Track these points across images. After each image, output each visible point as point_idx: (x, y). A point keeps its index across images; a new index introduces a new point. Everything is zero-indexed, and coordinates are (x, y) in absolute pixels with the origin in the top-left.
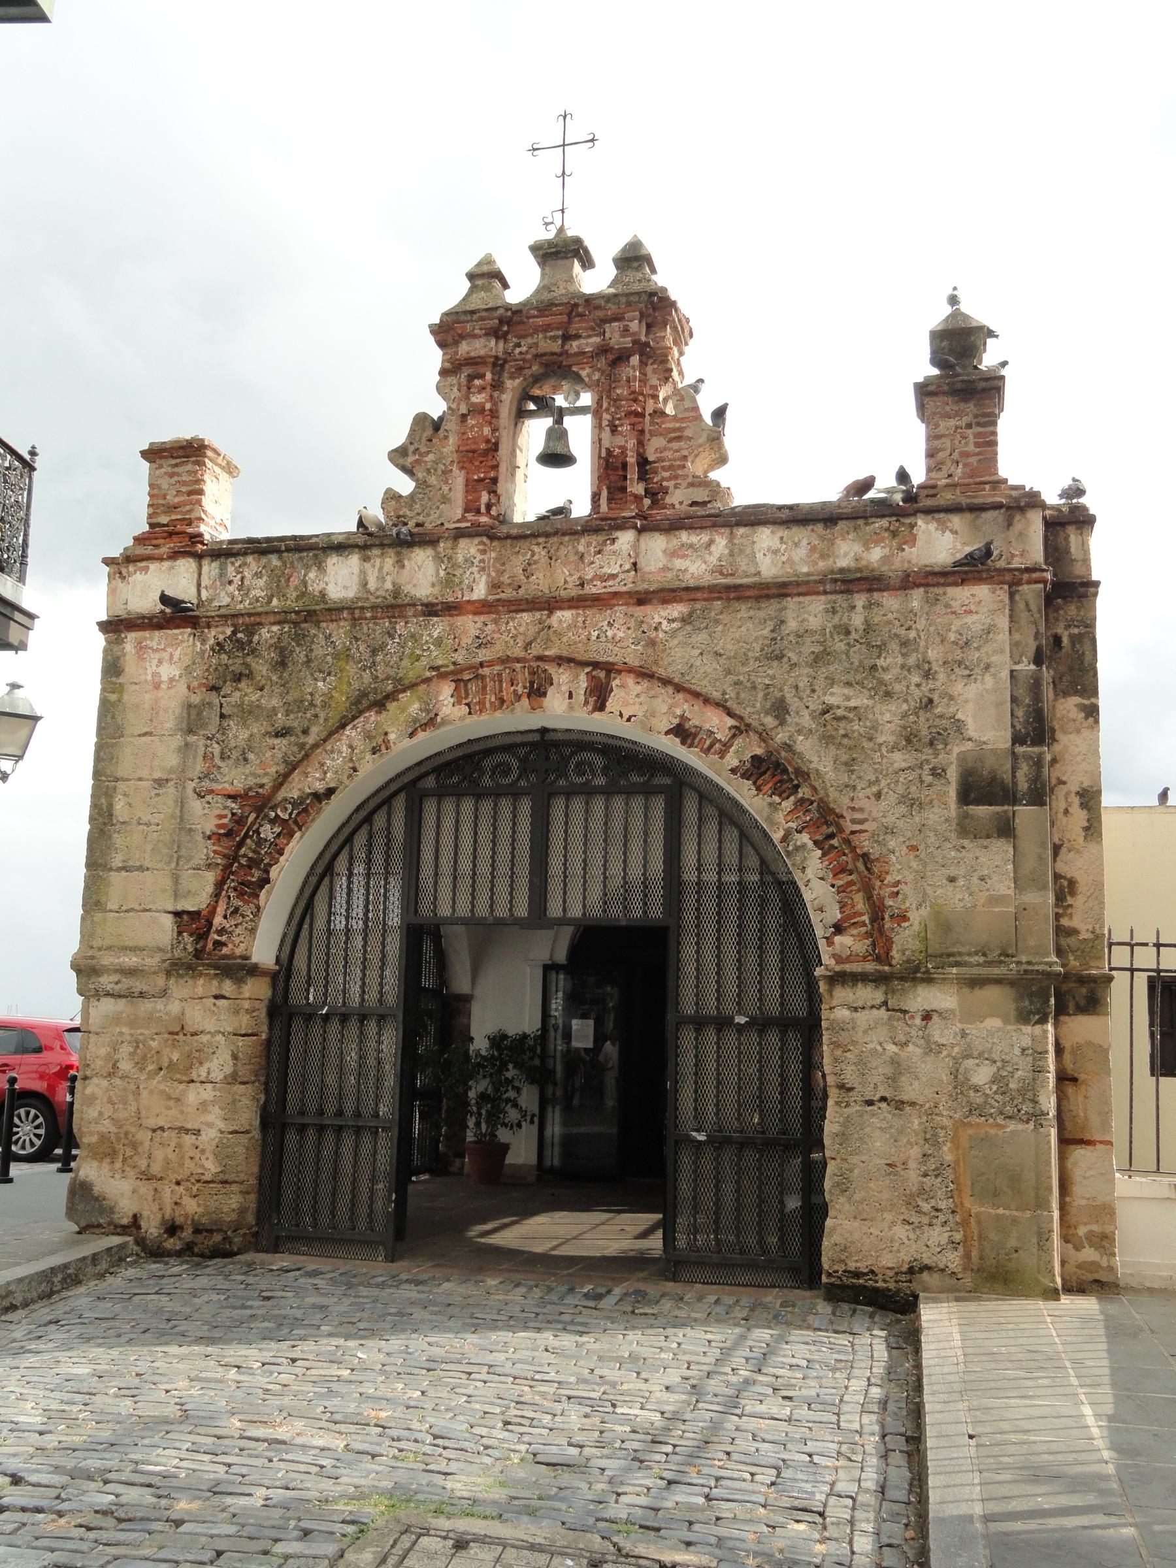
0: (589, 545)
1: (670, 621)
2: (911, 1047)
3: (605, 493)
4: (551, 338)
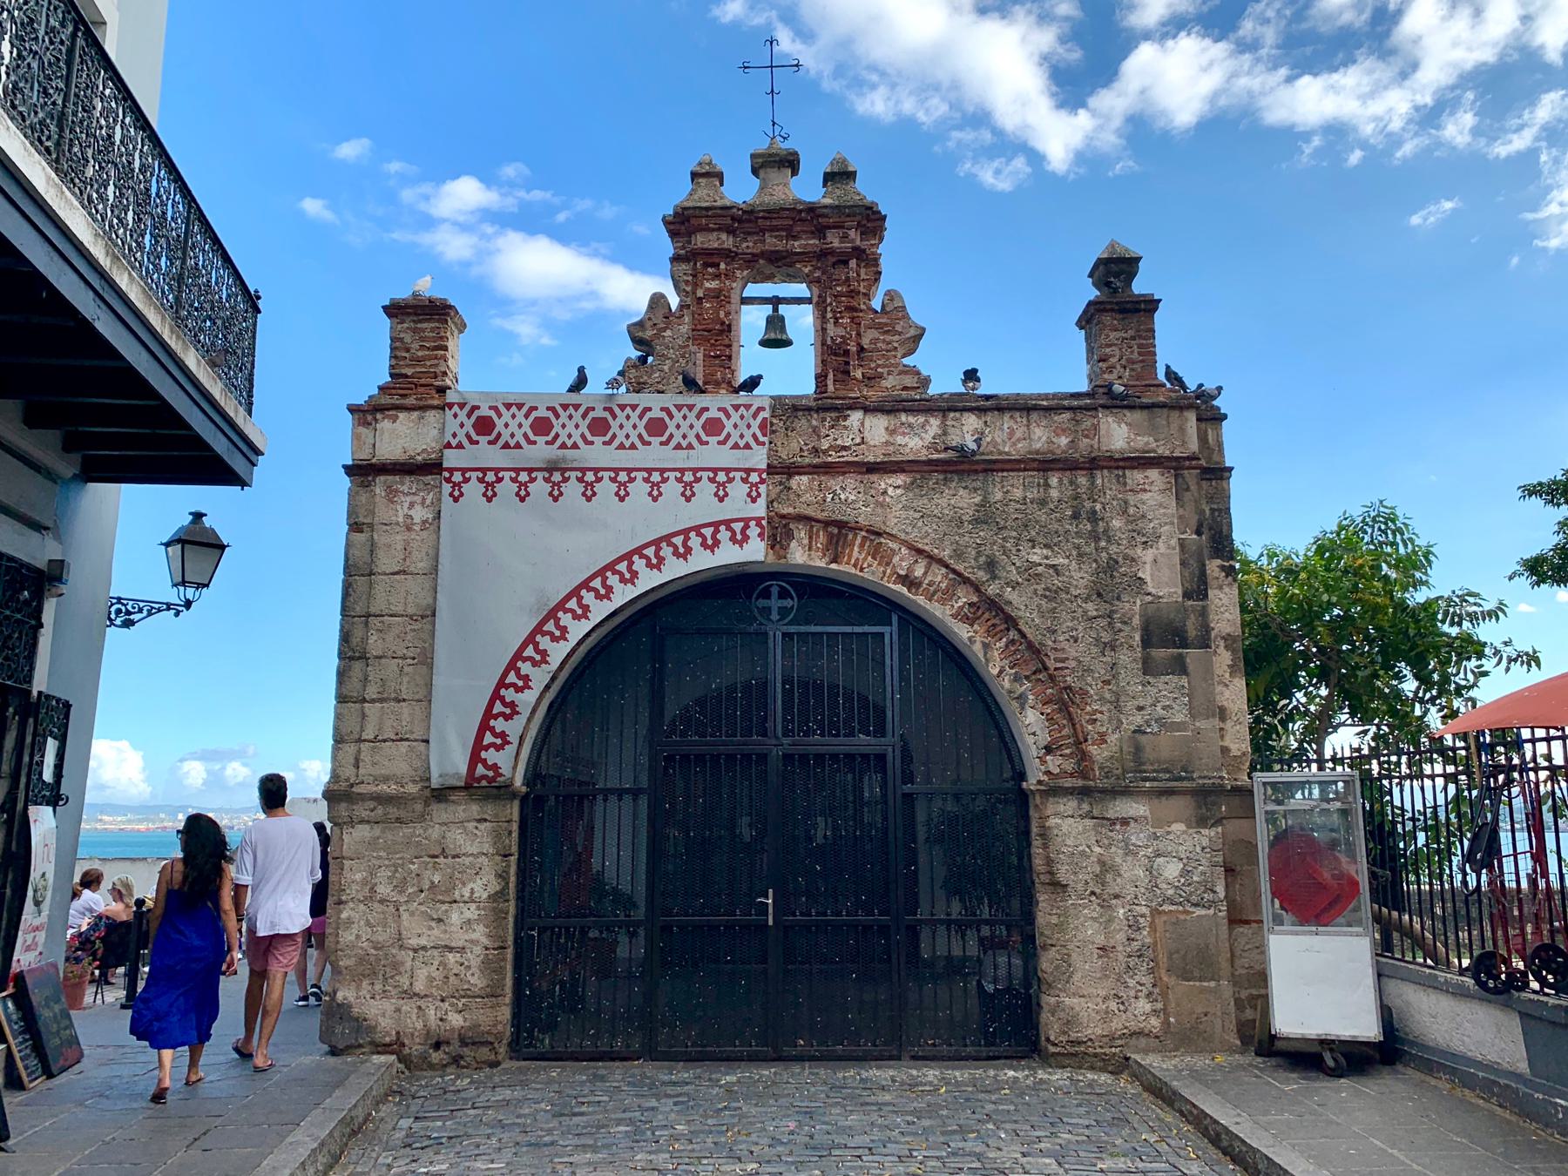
2: (1113, 849)
3: (831, 376)
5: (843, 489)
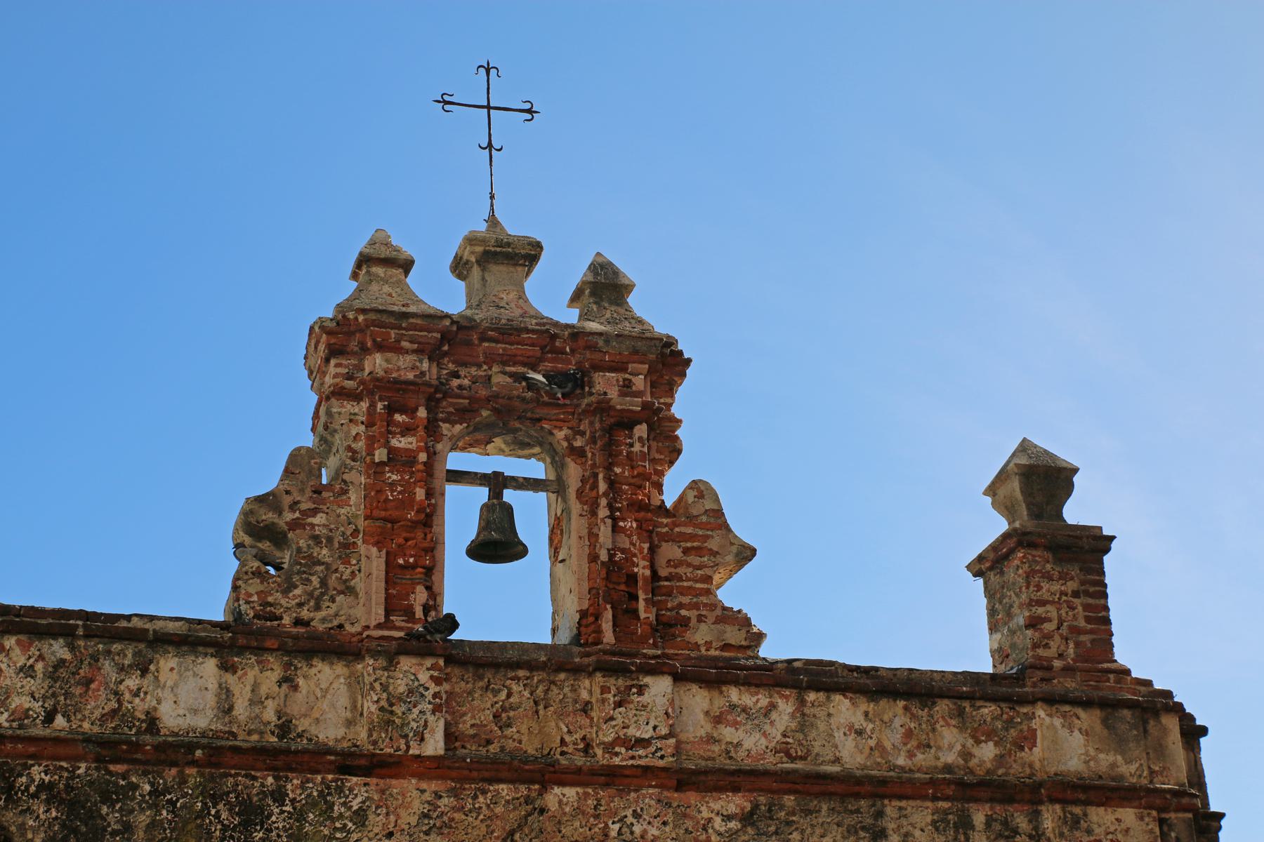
0: (605, 690)
1: (728, 818)
4: (511, 375)
5: (636, 815)
